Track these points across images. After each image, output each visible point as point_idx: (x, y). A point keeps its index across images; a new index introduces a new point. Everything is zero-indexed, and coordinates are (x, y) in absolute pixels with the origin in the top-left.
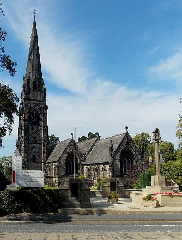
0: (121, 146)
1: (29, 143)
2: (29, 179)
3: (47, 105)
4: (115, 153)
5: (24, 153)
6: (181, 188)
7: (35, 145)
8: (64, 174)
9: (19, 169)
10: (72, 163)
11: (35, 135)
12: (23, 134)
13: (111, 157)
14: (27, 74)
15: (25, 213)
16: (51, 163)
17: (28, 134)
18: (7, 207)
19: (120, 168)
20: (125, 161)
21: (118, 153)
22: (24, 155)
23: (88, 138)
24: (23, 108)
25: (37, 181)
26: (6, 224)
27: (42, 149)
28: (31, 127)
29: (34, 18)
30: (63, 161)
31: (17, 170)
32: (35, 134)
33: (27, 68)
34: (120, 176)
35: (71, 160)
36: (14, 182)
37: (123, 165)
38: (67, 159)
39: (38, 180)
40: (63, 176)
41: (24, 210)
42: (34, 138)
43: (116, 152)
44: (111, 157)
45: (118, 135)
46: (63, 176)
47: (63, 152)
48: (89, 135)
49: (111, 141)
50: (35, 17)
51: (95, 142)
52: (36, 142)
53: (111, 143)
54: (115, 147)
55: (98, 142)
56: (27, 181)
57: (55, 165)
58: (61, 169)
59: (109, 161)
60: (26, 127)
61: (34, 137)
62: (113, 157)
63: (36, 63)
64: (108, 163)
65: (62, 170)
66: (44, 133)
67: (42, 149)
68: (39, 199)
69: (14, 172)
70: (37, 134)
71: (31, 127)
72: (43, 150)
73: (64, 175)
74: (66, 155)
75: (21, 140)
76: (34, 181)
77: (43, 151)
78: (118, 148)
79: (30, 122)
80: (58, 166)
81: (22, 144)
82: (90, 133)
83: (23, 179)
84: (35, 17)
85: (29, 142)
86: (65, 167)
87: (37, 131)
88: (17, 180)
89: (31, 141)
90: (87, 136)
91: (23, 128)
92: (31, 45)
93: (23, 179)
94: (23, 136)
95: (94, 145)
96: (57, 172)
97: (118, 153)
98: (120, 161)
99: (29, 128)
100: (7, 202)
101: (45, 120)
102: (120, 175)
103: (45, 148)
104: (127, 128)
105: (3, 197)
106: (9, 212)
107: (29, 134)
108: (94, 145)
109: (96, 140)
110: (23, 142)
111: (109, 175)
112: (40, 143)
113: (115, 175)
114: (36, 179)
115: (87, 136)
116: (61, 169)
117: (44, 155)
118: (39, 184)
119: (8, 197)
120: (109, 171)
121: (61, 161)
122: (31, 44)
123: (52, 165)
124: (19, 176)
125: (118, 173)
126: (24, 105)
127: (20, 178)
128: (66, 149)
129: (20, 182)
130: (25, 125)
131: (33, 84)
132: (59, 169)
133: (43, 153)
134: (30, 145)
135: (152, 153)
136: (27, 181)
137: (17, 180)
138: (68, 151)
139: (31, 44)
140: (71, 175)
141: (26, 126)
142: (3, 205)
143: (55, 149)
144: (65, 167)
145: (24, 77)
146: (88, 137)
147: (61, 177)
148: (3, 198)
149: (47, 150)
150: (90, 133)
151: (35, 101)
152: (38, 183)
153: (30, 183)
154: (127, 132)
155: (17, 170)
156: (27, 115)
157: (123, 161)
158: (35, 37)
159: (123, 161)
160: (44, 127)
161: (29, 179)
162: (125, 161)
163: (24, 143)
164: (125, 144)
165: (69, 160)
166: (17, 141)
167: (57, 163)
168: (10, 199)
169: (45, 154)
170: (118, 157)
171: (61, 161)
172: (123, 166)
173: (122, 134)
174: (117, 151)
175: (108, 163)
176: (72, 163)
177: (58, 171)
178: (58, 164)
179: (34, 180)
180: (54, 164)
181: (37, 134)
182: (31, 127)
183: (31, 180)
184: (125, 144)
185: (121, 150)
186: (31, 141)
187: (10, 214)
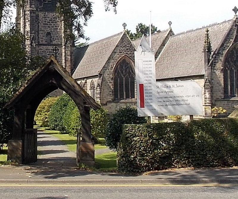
0: (225, 44)
1: (39, 45)
2: (171, 99)
4: (215, 57)
8: (110, 98)
9: (150, 79)
10: (124, 79)
13: (208, 64)
15: (179, 168)
16: (84, 78)
17: (37, 28)
18: (142, 155)
19: (223, 85)
20: (232, 71)
21: (221, 58)
23: (136, 35)
25: (188, 102)
26: (158, 190)
27: (64, 54)
28: (41, 15)
30: (109, 75)
31: (146, 82)
32: (49, 27)
34: (224, 99)
35: (123, 73)
36: (142, 106)
37: (229, 80)
38: (116, 71)
39: (190, 101)
40: (110, 102)
41: (178, 162)
42: (49, 34)
43: (216, 55)
44: (208, 64)
45: (215, 25)
46: (110, 102)
47: (109, 59)
48: (137, 29)
49: (208, 35)
51: (166, 39)
52: (51, 41)
53: (208, 38)
54: (215, 46)
55: (171, 39)
56: (167, 103)
57: (92, 83)
58: (106, 90)
59: (203, 72)
60: (33, 15)
62: (211, 64)
64: (201, 77)
65: (106, 91)
67: (64, 54)
68: (209, 138)
69: (141, 86)
70: (53, 27)
71: (41, 15)
72: (65, 56)
73: (111, 101)
74: (113, 64)
76: (182, 103)
77: (65, 59)
78: (221, 47)
79: (41, 5)
80: (100, 84)
81: (27, 46)
82: (141, 25)
83: (160, 100)
85: (39, 42)
86: (111, 87)
88: (149, 101)
89: (43, 39)
90: (134, 31)
93: (160, 100)
95: (163, 44)
96: (99, 96)
97: (221, 58)
98: (224, 71)
99: (38, 16)
100: (144, 146)
102: (223, 97)
103: (69, 53)
105: (134, 137)
106: (146, 166)
107: (38, 27)
108: (163, 44)
109: (168, 35)
111: (205, 98)
112: (59, 43)
113: (215, 98)
114: (185, 98)
115: (134, 31)
116: (106, 90)
117: (68, 65)
118: (193, 109)
119: (145, 136)
120: (205, 91)
121: (105, 76)
123: (86, 82)
124: (151, 93)
125: (220, 94)
127: (154, 99)
128: (114, 52)
129: (155, 106)
130: (31, 12)
132: (102, 90)
133: (65, 63)
134: (41, 47)
136: (167, 103)
137: (149, 101)
138: (118, 57)
140: (123, 100)
141: (34, 13)
142: (133, 152)
143: (86, 54)
144: (111, 87)
146: (136, 33)
147: (106, 104)
148: (135, 139)
150: (141, 25)
152: (190, 107)
153: (175, 108)
155: (146, 82)
157: (229, 71)
159: (229, 71)
161: (171, 99)
162: (232, 71)
164: (233, 40)
165: (118, 73)
167: (98, 78)
168: (149, 140)
169: (68, 64)
170: (219, 65)
171: (106, 75)
174: (218, 53)
175: (201, 77)
176: (124, 79)
177: (101, 93)
178: (100, 81)
179: (183, 100)
180: (89, 81)
181: (53, 27)
182: (43, 15)
183: (176, 102)
184: (232, 41)
185: (225, 52)
186: (43, 39)
187: (149, 170)
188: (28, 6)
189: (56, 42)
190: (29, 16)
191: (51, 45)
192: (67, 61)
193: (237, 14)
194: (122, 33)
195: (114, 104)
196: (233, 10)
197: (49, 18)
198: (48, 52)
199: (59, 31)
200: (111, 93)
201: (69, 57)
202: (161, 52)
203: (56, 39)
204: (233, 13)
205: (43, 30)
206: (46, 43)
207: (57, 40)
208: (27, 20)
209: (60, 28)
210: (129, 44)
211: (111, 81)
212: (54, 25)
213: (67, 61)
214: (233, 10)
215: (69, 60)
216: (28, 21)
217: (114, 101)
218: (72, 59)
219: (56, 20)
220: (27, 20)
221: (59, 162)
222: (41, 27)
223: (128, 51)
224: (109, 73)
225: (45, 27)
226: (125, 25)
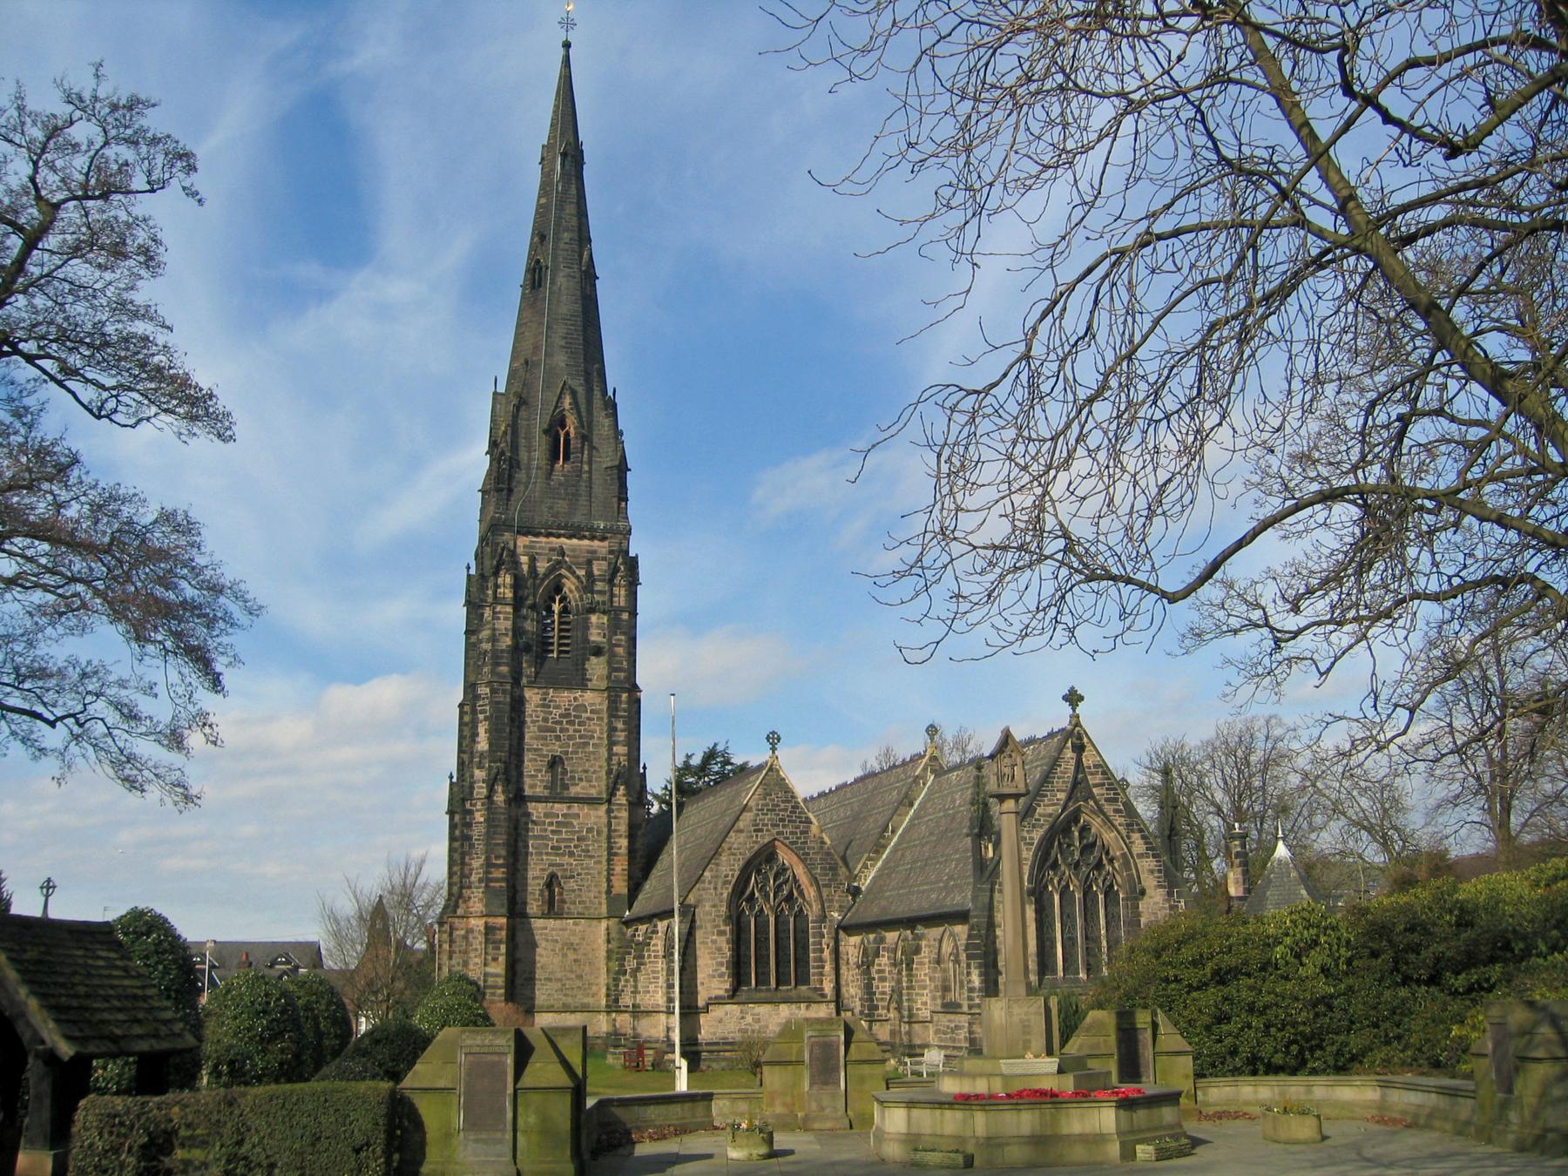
3: (637, 557)
5: (488, 859)
6: (6, 680)
7: (560, 808)
11: (557, 749)
12: (483, 744)
14: (512, 374)
22: (487, 872)
24: (482, 577)
29: (562, 51)
32: (558, 738)
33: (532, 239)
50: (567, 45)
52: (565, 787)
61: (554, 757)
63: (567, 306)
66: (615, 729)
70: (570, 738)
75: (472, 776)
84: (567, 45)
87: (571, 723)
91: (484, 706)
92: (539, 206)
94: (482, 754)
101: (620, 651)
104: (1073, 698)
110: (481, 790)
120: (969, 966)
122: (539, 197)
126: (489, 564)
131: (546, 432)
135: (1243, 846)
139: (543, 201)
145: (495, 393)
149: (631, 837)
151: (559, 536)
154: (1078, 724)
156: (509, 624)
158: (567, 62)
160: (613, 691)
163: (489, 797)
166: (452, 784)
172: (1058, 926)
173: (1051, 735)
181: (570, 738)
188: (485, 669)
189: (583, 788)
190: (487, 701)
191: (562, 800)
192: (616, 854)
193: (1078, 710)
194: (921, 757)
195: (735, 1007)
196: (1065, 698)
197: (558, 707)
198: (551, 824)
199: (594, 753)
200: (724, 969)
201: (624, 842)
202: (898, 828)
203: (581, 779)
204: (1066, 709)
205: (536, 750)
206: (546, 793)
207: (584, 783)
208: (481, 717)
209: (596, 741)
210: (789, 802)
211: (723, 928)
212: (575, 731)
213: (616, 854)
214: (1065, 698)
215: (624, 851)
216: (486, 719)
217: (733, 995)
218: (638, 845)
219: (584, 715)
220: (481, 717)
221: (116, 982)
222: (532, 738)
223: (784, 826)
224: (717, 902)
225: (545, 738)
226: (932, 730)
